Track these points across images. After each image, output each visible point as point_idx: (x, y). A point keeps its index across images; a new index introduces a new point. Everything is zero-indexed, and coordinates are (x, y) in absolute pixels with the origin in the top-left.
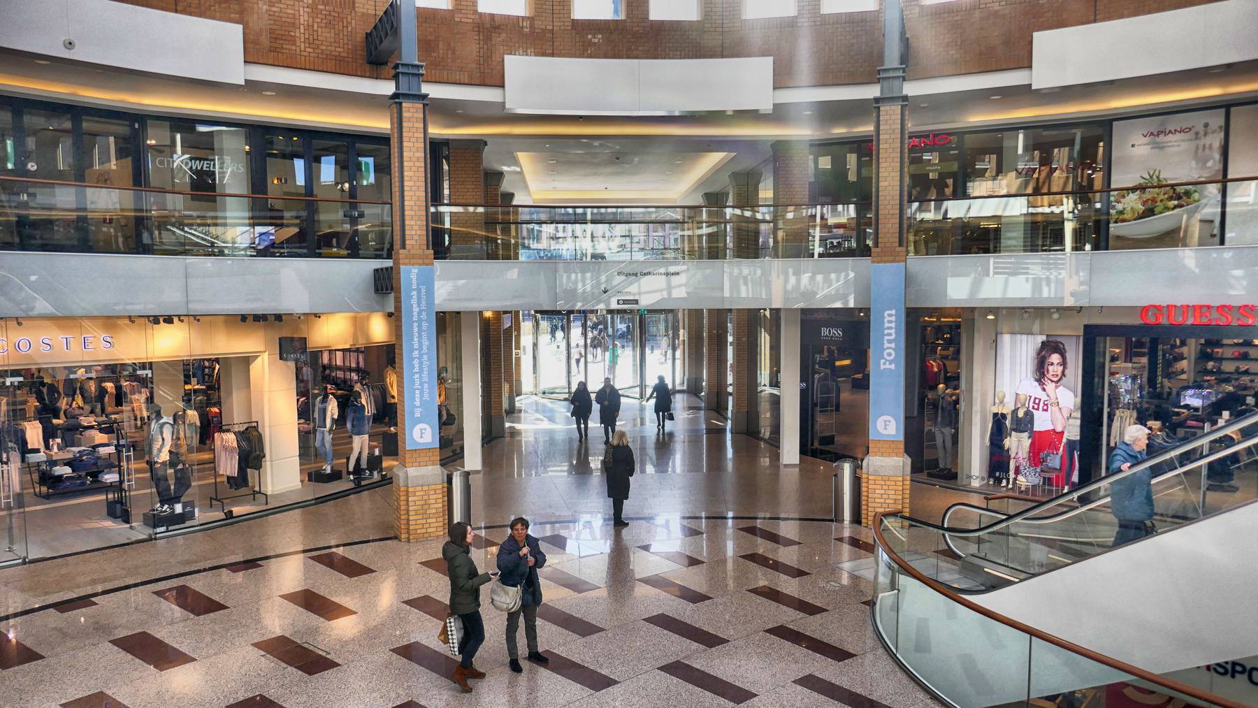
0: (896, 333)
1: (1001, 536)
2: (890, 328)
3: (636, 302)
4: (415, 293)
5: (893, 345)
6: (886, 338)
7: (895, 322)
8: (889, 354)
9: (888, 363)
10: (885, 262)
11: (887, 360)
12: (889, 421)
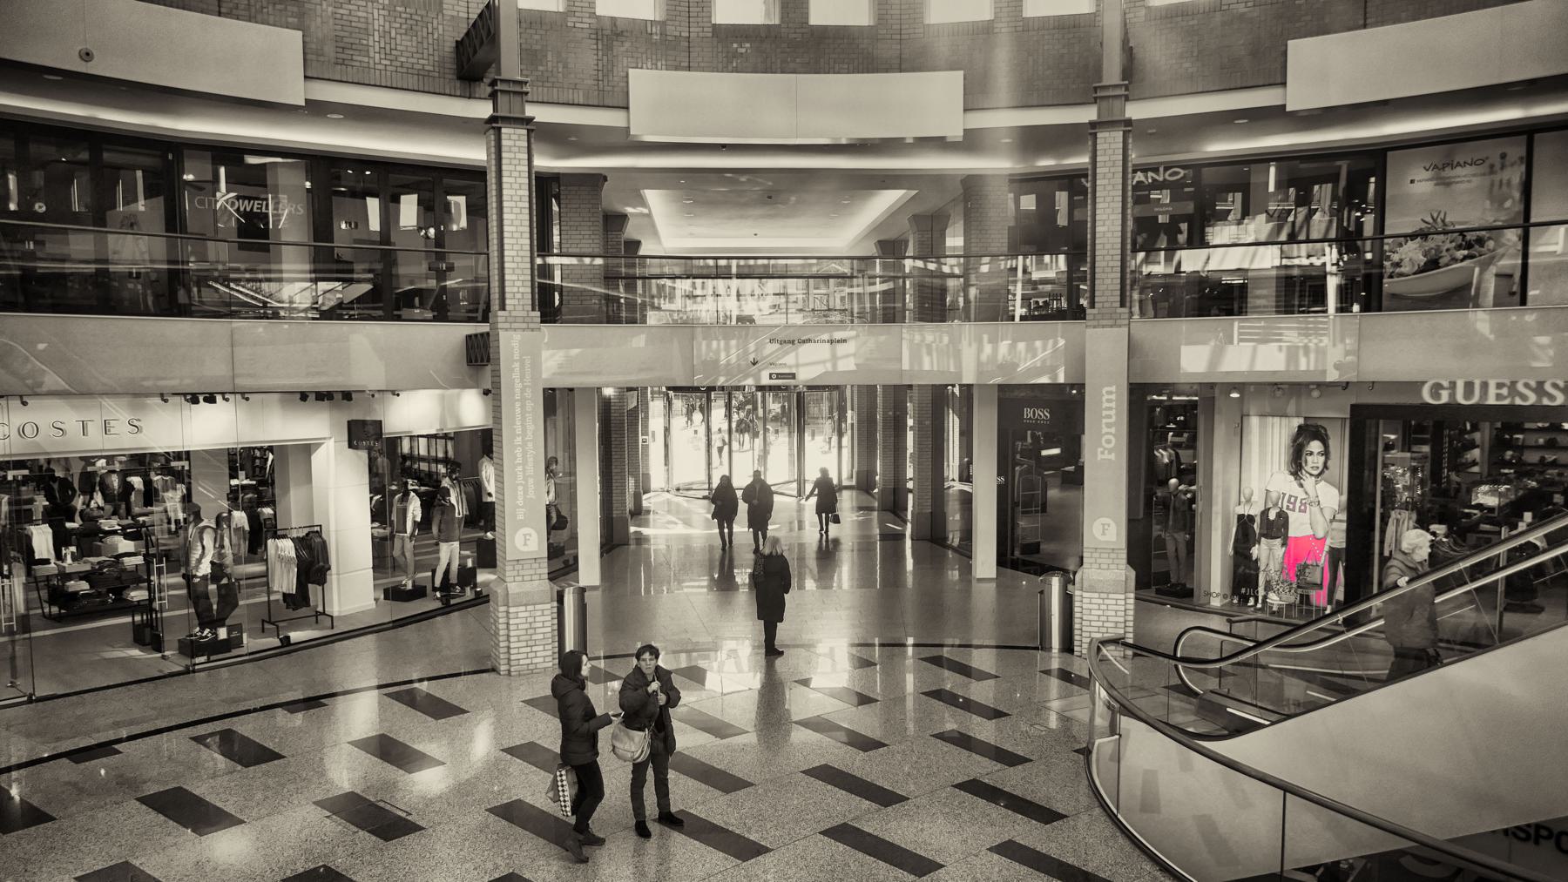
3: (793, 376)
4: (517, 365)
6: (1104, 421)
11: (1105, 449)
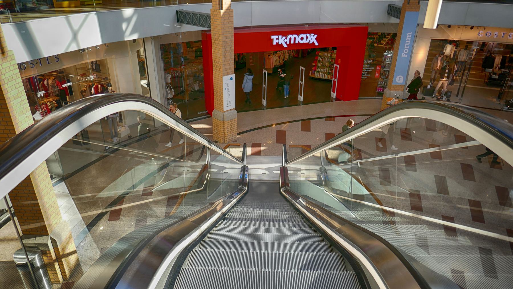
1: (20, 105)
2: (408, 40)
8: (406, 51)
9: (405, 54)
11: (404, 53)
12: (401, 78)
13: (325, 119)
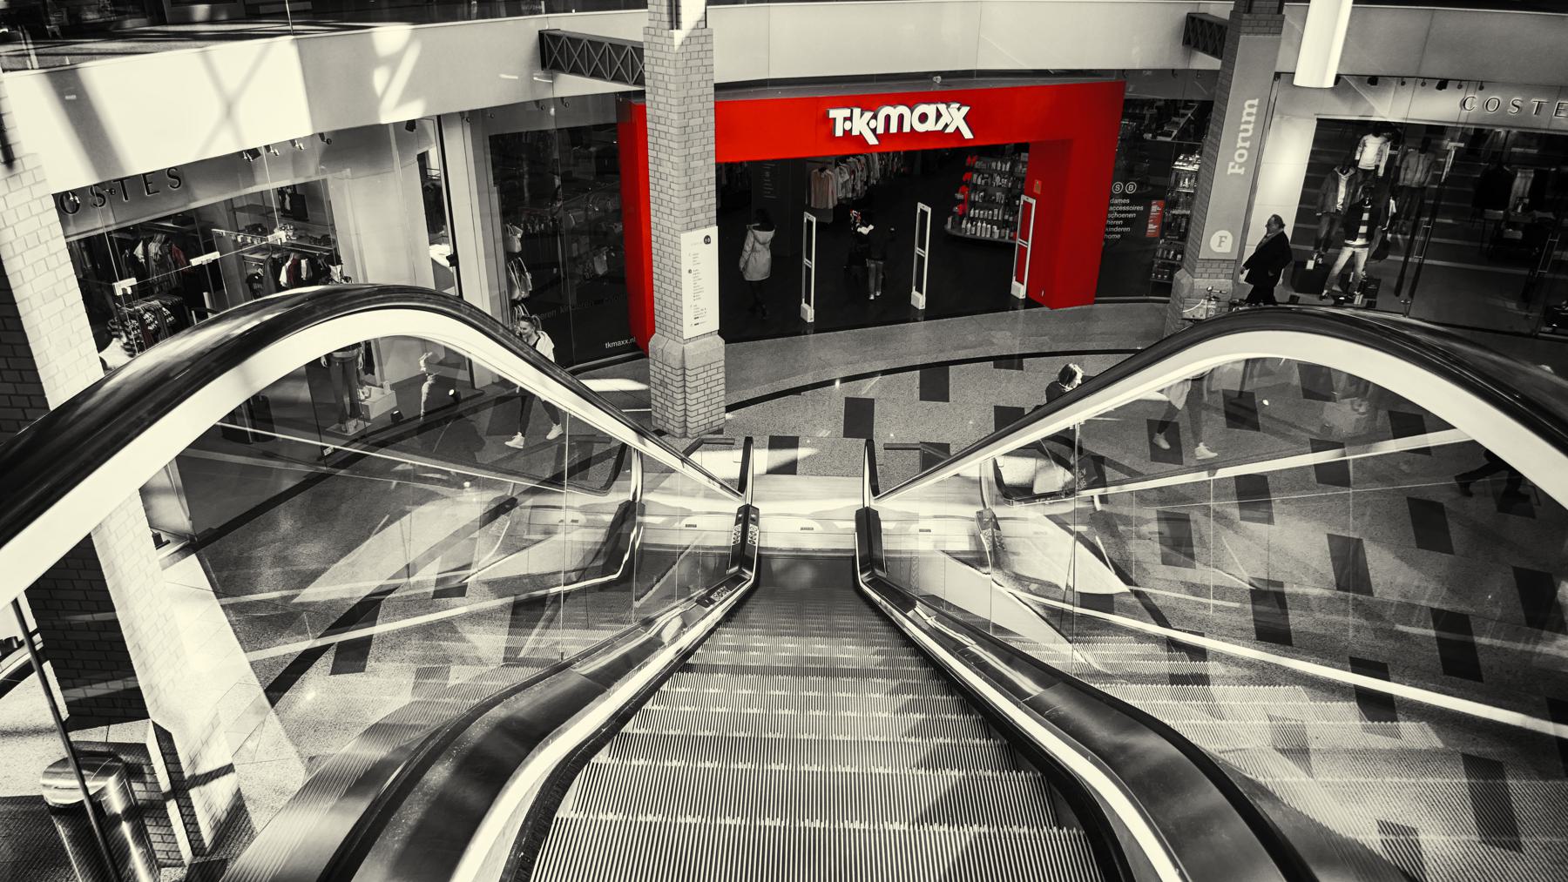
0: (1254, 129)
2: (1248, 122)
5: (1247, 144)
7: (1255, 122)
8: (1241, 156)
9: (1237, 166)
10: (1257, 34)
11: (1236, 163)
13: (918, 371)
